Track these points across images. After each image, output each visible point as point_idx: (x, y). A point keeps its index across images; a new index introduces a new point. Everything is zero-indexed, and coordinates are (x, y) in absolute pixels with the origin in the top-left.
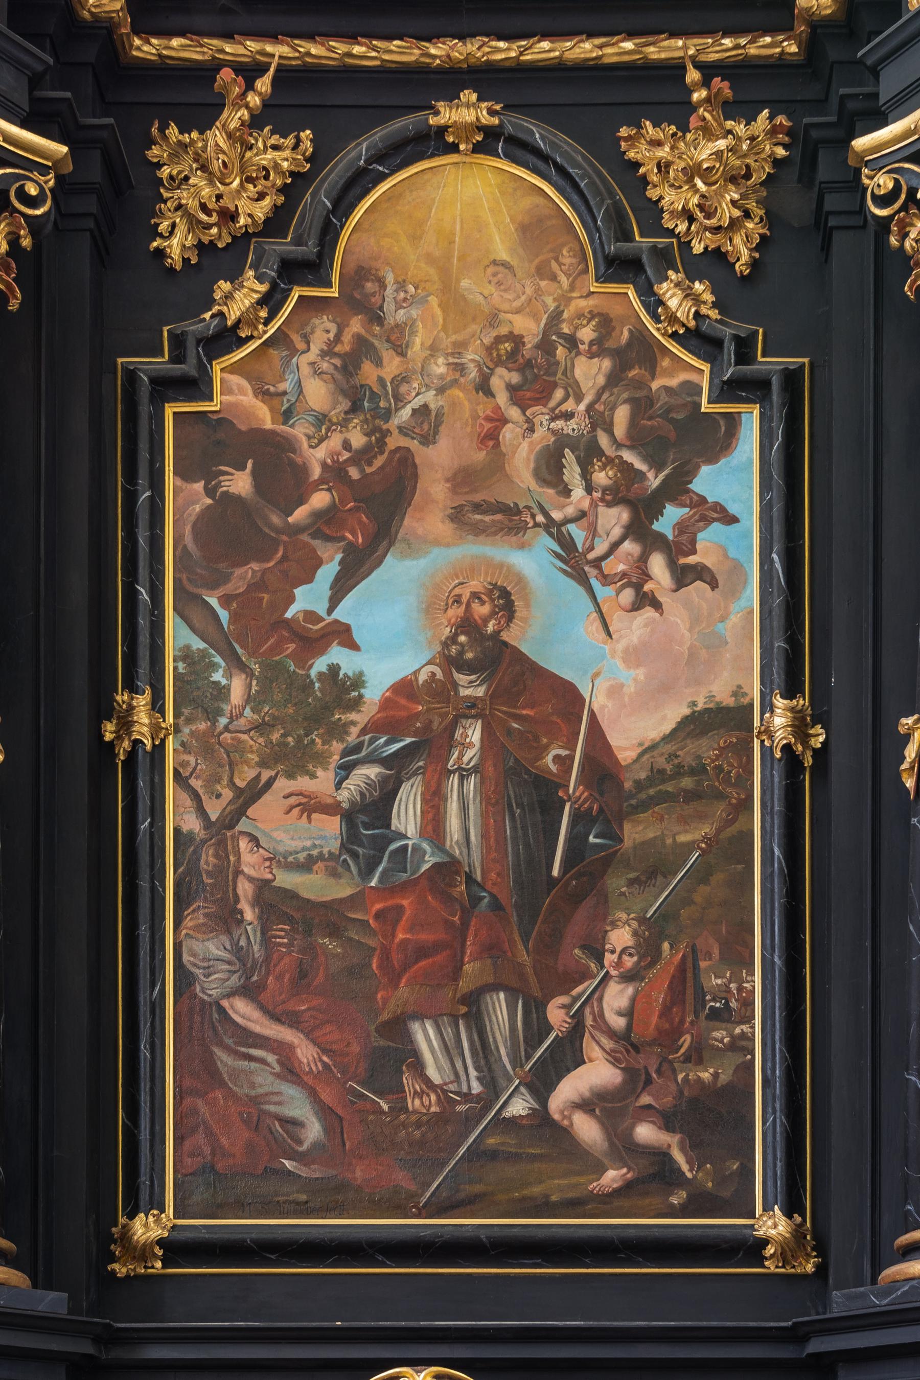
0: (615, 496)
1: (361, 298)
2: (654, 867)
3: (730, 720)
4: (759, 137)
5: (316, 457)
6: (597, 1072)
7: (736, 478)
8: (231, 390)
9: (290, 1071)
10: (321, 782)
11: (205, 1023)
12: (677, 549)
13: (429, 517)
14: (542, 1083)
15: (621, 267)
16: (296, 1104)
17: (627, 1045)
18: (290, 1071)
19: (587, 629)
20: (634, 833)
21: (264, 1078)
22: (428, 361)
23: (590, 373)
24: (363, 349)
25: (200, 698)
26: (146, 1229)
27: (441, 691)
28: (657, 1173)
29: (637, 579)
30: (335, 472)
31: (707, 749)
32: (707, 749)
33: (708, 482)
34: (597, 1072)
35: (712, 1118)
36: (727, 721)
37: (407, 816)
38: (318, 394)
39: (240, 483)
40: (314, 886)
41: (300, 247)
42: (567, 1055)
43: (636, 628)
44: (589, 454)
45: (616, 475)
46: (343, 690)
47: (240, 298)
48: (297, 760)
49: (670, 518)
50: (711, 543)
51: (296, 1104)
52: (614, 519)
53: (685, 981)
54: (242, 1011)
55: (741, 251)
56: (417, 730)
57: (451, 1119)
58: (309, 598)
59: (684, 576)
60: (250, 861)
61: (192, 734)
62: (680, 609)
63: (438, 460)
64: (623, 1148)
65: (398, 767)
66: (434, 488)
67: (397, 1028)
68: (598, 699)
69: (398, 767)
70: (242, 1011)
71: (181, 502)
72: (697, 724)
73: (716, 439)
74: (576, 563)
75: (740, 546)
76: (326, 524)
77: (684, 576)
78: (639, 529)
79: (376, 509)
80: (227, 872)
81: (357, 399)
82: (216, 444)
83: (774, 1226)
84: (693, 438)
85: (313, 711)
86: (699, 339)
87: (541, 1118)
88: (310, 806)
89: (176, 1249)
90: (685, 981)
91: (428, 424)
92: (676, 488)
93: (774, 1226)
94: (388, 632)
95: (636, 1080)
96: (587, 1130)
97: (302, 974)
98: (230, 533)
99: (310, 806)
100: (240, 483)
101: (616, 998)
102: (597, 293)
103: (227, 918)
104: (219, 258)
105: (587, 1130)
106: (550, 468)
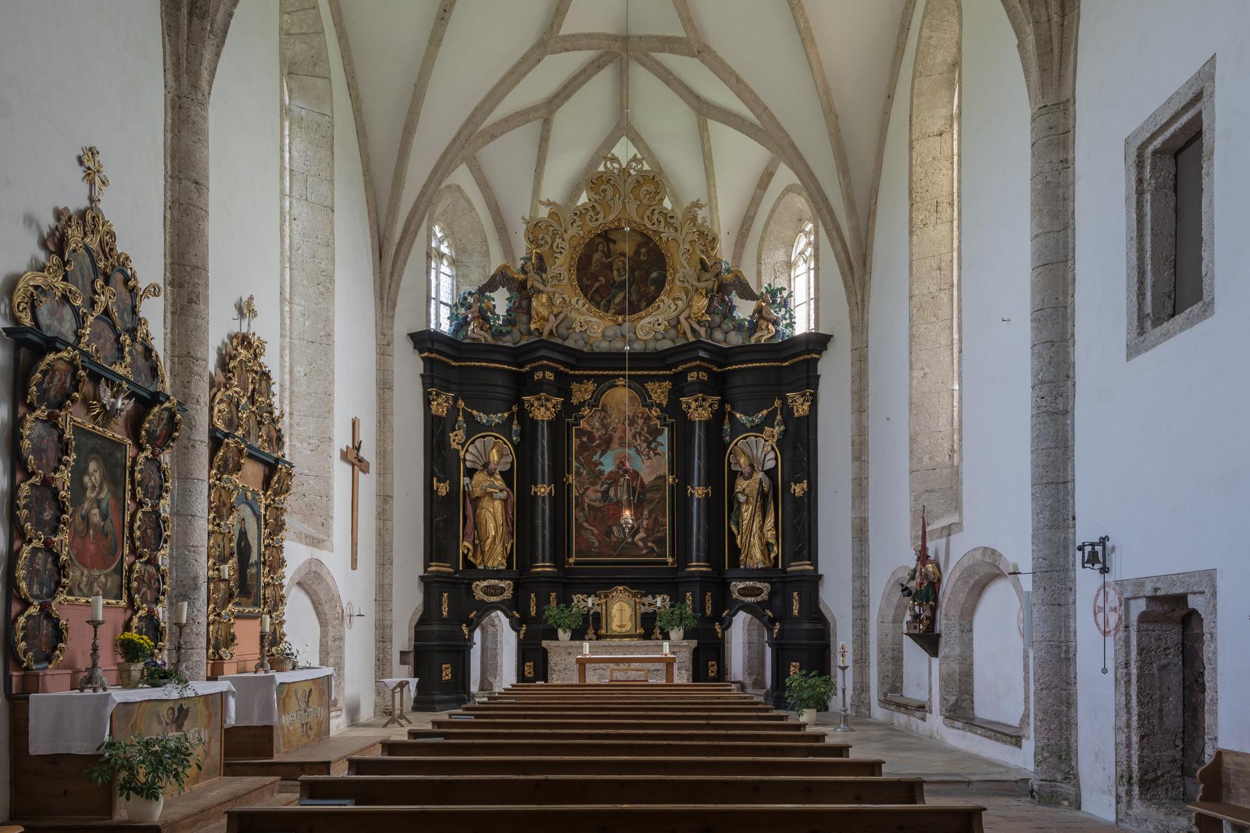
0: (644, 441)
1: (604, 410)
2: (651, 501)
3: (663, 477)
4: (667, 385)
5: (597, 435)
6: (642, 534)
7: (664, 439)
8: (583, 424)
9: (593, 534)
10: (598, 487)
11: (579, 526)
12: (654, 450)
13: (615, 445)
14: (633, 536)
15: (644, 406)
16: (594, 540)
17: (647, 530)
18: (593, 534)
19: (640, 463)
20: (648, 496)
21: (589, 535)
22: (614, 419)
23: (640, 421)
24: (604, 418)
25: (578, 474)
26: (571, 560)
27: (617, 473)
28: (651, 551)
29: (648, 455)
30: (600, 437)
31: (659, 482)
32: (659, 482)
33: (659, 439)
34: (642, 534)
35: (660, 542)
36: (662, 478)
37: (612, 493)
38: (597, 425)
39: (585, 439)
40: (597, 504)
41: (594, 402)
42: (637, 532)
43: (648, 463)
44: (640, 434)
45: (637, 253)
46: (601, 472)
47: (1066, 803)
48: (594, 484)
49: (653, 445)
50: (659, 450)
51: (594, 540)
52: (644, 445)
53: (656, 520)
54: (585, 524)
55: (665, 403)
56: (613, 479)
57: (619, 542)
58: (596, 458)
59: (655, 454)
60: (587, 500)
61: (141, 619)
62: (655, 460)
63: (616, 436)
64: (646, 547)
65: (610, 485)
66: (616, 440)
67: (610, 527)
68: (642, 474)
69: (610, 485)
70: (585, 524)
71: (575, 442)
72: (658, 478)
73: (660, 432)
74: (638, 452)
75: (665, 449)
76: (598, 446)
77: (655, 454)
78: (648, 447)
79: (607, 444)
80: (583, 502)
81: (604, 426)
82: (581, 433)
83: (670, 560)
84: (656, 432)
85: (596, 476)
86: (658, 418)
87: (633, 543)
88: (596, 491)
89: (576, 563)
90: (656, 520)
91: (615, 430)
92: (654, 440)
93: (670, 560)
94: (608, 464)
95: (648, 536)
96: (641, 544)
97: (595, 519)
98: (583, 447)
99: (596, 491)
100: (585, 439)
101: (645, 522)
102: (641, 409)
103: (583, 510)
104: (582, 404)
105: (641, 544)
106: (634, 437)
